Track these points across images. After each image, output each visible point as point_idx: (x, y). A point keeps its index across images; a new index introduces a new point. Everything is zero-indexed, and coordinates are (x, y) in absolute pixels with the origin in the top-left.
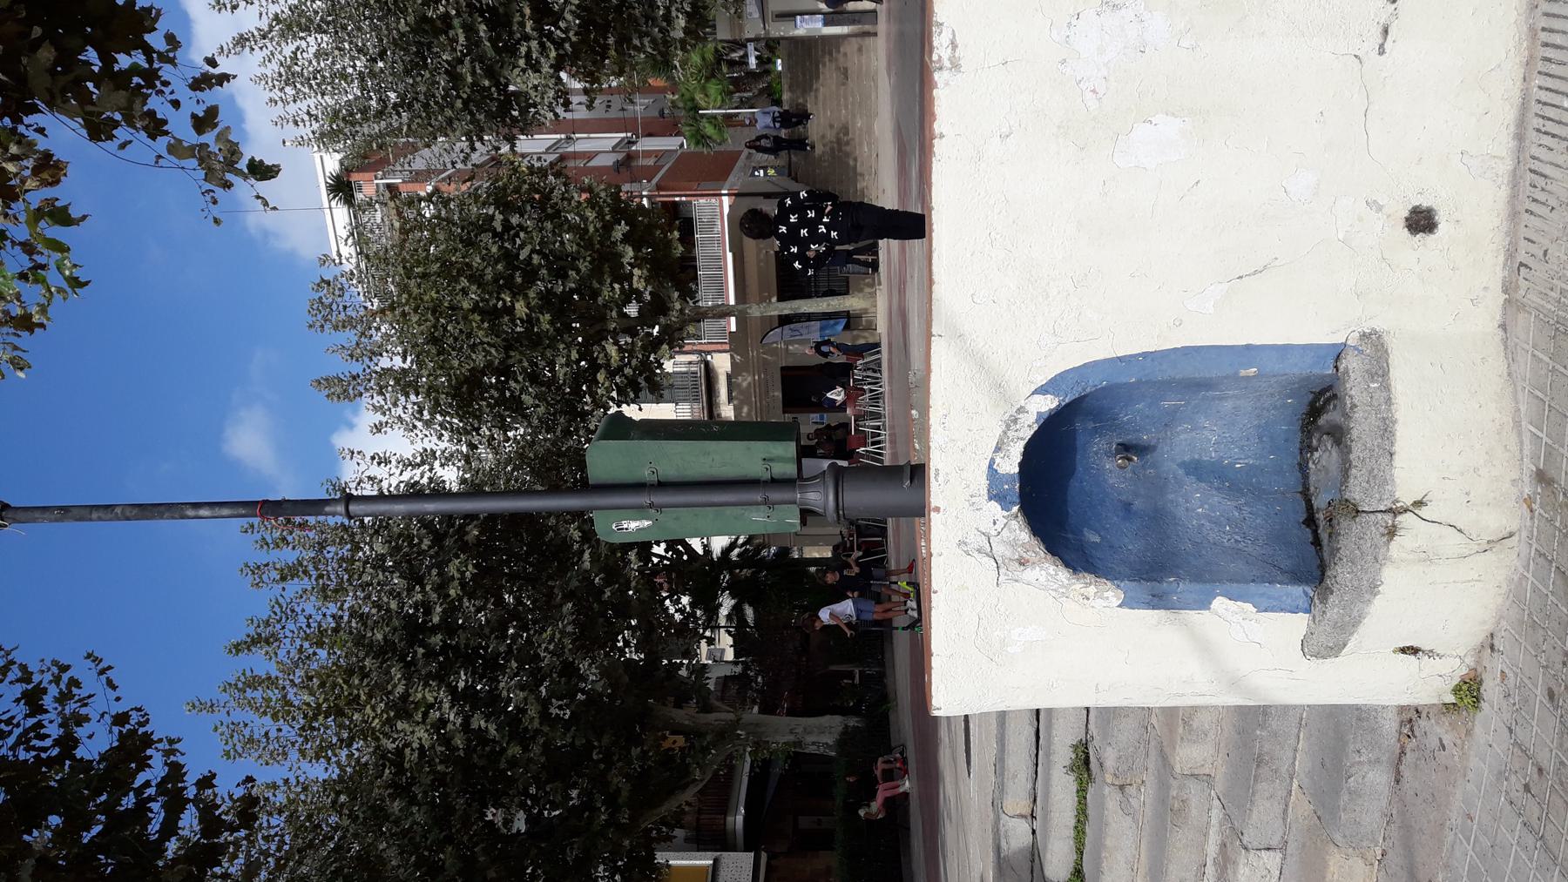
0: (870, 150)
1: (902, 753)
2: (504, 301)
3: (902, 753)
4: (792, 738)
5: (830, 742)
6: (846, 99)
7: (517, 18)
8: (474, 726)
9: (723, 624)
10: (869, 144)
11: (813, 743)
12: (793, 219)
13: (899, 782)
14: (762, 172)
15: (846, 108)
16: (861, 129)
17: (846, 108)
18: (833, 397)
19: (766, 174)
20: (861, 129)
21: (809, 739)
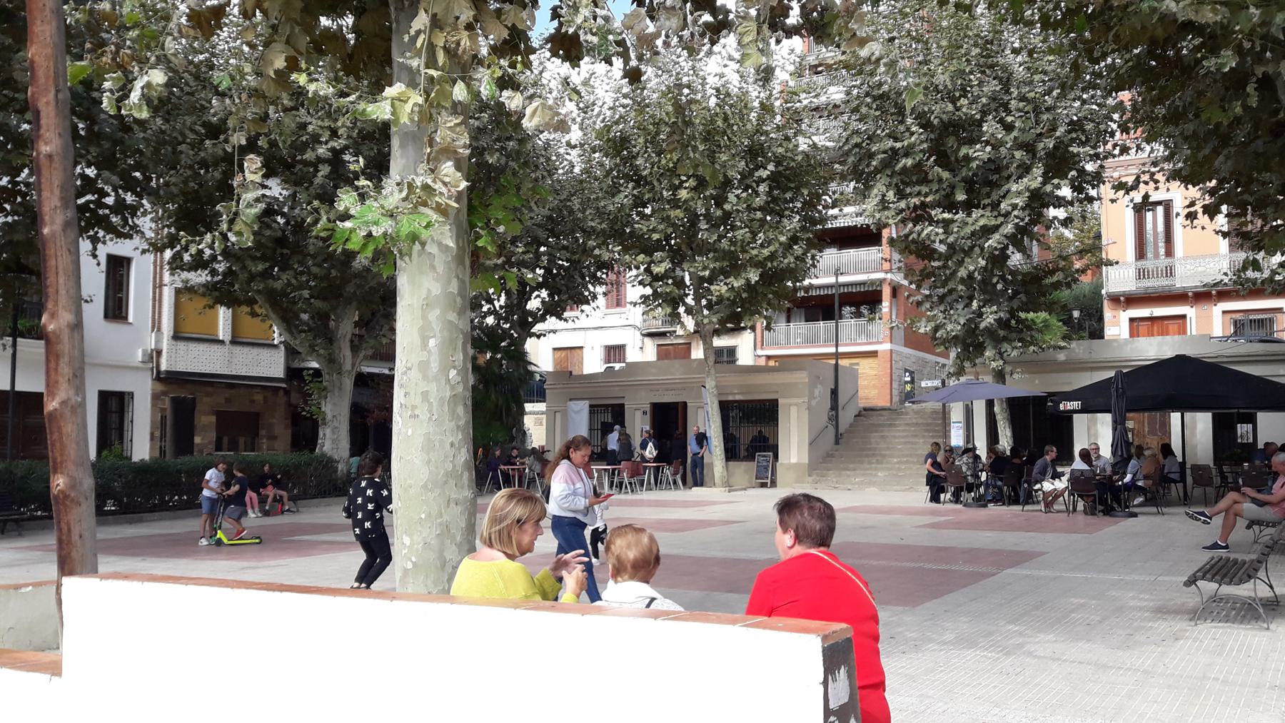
0: (856, 483)
1: (288, 510)
2: (686, 181)
3: (288, 510)
4: (329, 417)
5: (325, 448)
6: (907, 462)
7: (925, 189)
8: (321, 167)
9: (114, 415)
10: (861, 483)
11: (324, 435)
12: (369, 492)
13: (257, 509)
14: (908, 379)
15: (898, 463)
16: (876, 475)
17: (898, 463)
18: (649, 448)
19: (907, 382)
20: (876, 475)
21: (328, 431)
